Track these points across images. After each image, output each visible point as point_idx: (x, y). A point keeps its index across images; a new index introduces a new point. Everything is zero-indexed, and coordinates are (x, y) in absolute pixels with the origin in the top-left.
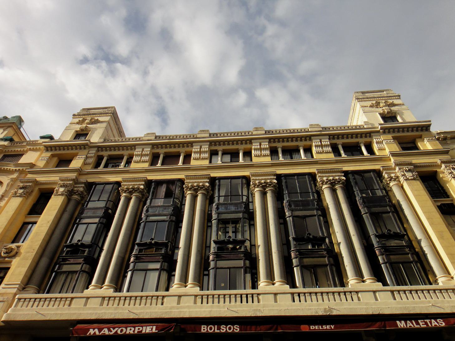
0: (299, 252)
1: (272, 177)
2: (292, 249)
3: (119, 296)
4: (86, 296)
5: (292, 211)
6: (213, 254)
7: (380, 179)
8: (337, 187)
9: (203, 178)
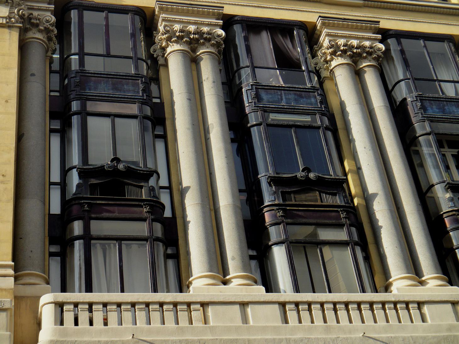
0: (285, 211)
1: (214, 21)
2: (266, 203)
3: (320, 300)
4: (239, 300)
5: (266, 111)
6: (451, 214)
7: (311, 48)
8: (201, 51)
9: (361, 29)
